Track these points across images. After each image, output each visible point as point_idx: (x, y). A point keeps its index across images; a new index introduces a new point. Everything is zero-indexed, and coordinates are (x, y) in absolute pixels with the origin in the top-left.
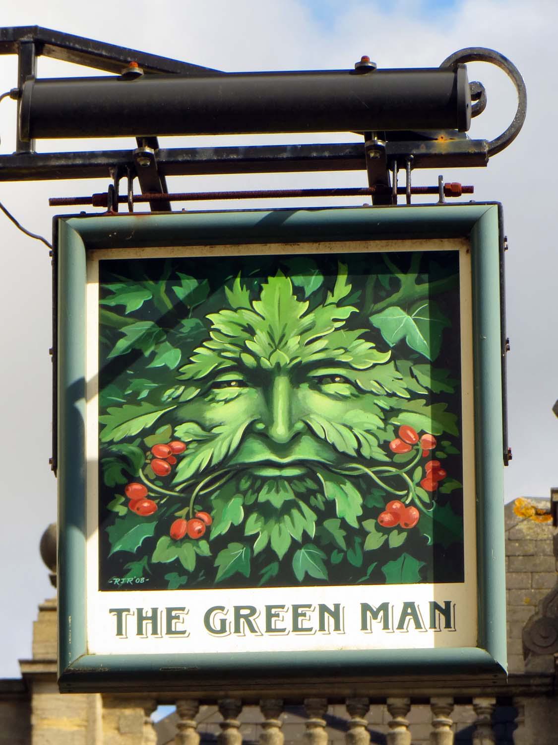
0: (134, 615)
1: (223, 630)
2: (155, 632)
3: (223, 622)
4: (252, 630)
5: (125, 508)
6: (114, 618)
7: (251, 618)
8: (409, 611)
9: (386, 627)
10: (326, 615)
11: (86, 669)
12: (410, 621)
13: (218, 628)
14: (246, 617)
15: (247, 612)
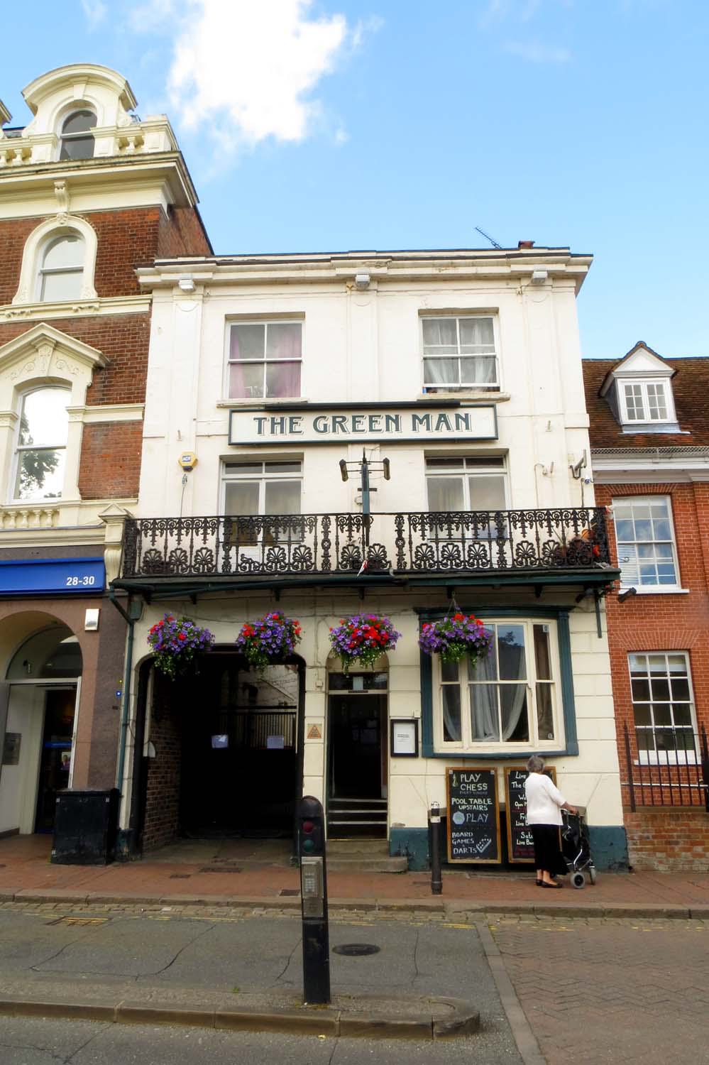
0: (428, 390)
1: (325, 430)
2: (282, 432)
3: (325, 426)
4: (344, 430)
5: (9, 732)
6: (257, 423)
7: (343, 423)
8: (443, 419)
9: (428, 429)
10: (460, 420)
11: (55, 1019)
12: (443, 426)
13: (322, 429)
14: (339, 423)
15: (341, 419)
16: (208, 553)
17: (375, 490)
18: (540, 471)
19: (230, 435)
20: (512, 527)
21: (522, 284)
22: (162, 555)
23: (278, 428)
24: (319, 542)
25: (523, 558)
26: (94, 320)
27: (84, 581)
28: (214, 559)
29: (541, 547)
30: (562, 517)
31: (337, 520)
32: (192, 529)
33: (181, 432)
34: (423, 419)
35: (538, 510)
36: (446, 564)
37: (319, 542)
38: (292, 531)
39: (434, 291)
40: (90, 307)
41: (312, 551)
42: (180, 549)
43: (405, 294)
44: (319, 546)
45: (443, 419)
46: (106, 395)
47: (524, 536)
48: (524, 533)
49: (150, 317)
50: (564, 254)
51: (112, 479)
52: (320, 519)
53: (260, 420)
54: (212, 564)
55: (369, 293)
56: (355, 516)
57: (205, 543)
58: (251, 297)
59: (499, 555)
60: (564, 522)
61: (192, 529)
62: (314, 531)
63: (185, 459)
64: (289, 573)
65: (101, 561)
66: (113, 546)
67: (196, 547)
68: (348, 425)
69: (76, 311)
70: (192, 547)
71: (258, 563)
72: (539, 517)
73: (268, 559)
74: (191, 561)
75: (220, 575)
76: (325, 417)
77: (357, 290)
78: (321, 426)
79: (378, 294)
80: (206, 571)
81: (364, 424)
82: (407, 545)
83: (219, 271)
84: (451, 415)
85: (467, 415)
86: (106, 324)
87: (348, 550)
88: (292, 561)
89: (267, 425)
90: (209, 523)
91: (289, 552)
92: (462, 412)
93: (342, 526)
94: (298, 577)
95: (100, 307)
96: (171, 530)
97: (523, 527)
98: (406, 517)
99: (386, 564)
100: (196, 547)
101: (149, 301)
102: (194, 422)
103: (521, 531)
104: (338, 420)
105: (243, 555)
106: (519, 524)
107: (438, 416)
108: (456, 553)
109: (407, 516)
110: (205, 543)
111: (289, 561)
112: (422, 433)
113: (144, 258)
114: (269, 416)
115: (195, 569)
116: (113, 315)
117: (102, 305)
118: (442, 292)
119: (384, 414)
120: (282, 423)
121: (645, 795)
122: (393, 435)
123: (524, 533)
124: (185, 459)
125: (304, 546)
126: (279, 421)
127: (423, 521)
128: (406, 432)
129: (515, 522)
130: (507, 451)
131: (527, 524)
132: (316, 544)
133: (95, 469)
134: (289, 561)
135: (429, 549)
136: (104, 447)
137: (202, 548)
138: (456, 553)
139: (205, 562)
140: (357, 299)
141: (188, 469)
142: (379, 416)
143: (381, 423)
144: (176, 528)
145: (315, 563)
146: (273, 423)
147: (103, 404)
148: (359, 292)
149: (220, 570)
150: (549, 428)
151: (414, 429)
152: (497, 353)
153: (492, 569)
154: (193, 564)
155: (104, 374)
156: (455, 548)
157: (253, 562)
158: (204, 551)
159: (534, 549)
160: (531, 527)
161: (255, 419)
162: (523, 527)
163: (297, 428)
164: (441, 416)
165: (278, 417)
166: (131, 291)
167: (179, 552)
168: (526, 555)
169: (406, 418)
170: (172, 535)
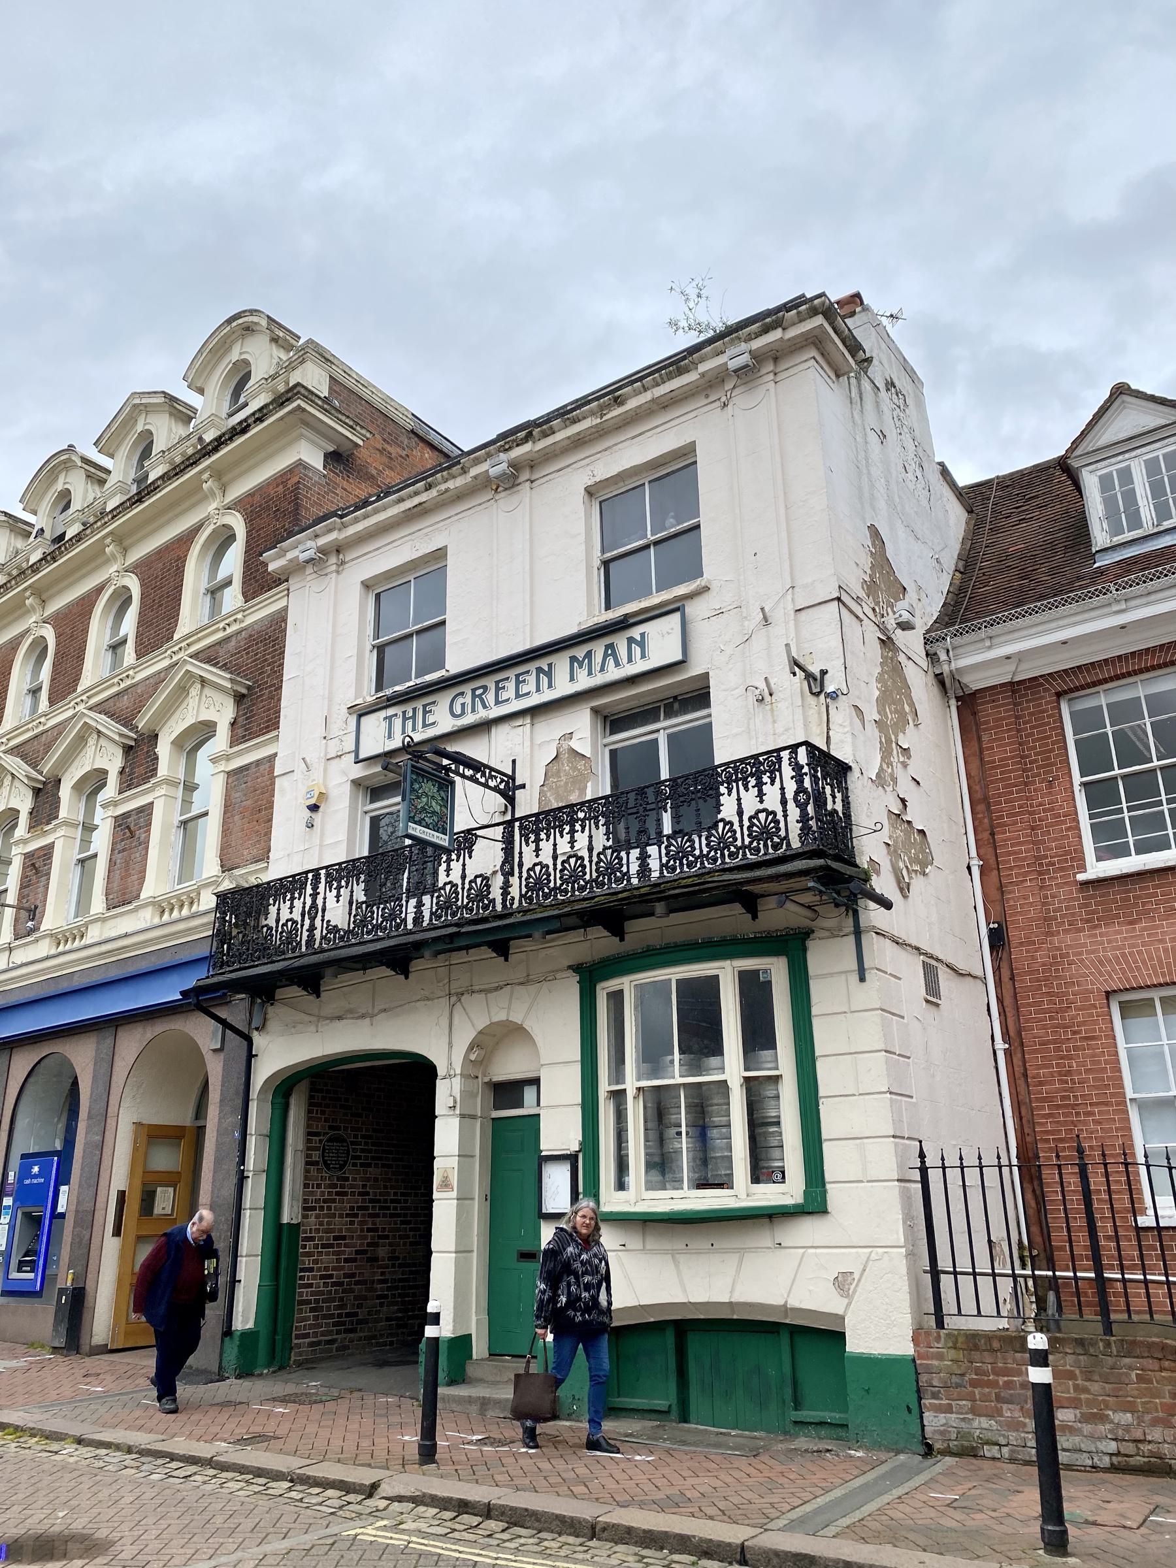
12: (611, 662)
14: (480, 696)
16: (770, 817)
17: (523, 786)
20: (467, 855)
21: (726, 389)
24: (790, 795)
28: (782, 825)
29: (746, 823)
30: (737, 776)
32: (736, 781)
33: (307, 759)
34: (584, 660)
35: (698, 772)
36: (566, 891)
37: (790, 795)
39: (605, 450)
40: (235, 621)
41: (780, 816)
42: (540, 863)
43: (569, 469)
44: (791, 805)
45: (610, 652)
52: (785, 755)
53: (389, 719)
54: (779, 837)
56: (682, 780)
57: (761, 801)
60: (740, 783)
61: (736, 781)
67: (748, 813)
69: (224, 629)
70: (740, 813)
74: (555, 881)
75: (411, 932)
77: (506, 489)
78: (458, 710)
79: (534, 484)
80: (727, 860)
81: (509, 691)
83: (344, 526)
84: (620, 642)
85: (643, 635)
88: (747, 840)
90: (720, 776)
91: (741, 826)
92: (636, 632)
94: (332, 953)
100: (748, 813)
101: (286, 592)
102: (324, 741)
104: (478, 692)
105: (329, 921)
107: (626, 641)
110: (761, 801)
111: (701, 851)
112: (584, 681)
118: (620, 446)
119: (532, 666)
121: (1109, 1225)
122: (548, 696)
125: (722, 820)
128: (564, 687)
130: (706, 676)
132: (784, 802)
134: (701, 851)
136: (244, 798)
137: (535, 865)
139: (765, 834)
140: (505, 502)
141: (314, 808)
144: (752, 775)
145: (787, 837)
148: (508, 492)
149: (410, 926)
150: (765, 619)
153: (630, 889)
154: (705, 850)
155: (247, 702)
156: (770, 817)
158: (762, 816)
163: (431, 719)
164: (607, 647)
167: (762, 816)
170: (747, 789)
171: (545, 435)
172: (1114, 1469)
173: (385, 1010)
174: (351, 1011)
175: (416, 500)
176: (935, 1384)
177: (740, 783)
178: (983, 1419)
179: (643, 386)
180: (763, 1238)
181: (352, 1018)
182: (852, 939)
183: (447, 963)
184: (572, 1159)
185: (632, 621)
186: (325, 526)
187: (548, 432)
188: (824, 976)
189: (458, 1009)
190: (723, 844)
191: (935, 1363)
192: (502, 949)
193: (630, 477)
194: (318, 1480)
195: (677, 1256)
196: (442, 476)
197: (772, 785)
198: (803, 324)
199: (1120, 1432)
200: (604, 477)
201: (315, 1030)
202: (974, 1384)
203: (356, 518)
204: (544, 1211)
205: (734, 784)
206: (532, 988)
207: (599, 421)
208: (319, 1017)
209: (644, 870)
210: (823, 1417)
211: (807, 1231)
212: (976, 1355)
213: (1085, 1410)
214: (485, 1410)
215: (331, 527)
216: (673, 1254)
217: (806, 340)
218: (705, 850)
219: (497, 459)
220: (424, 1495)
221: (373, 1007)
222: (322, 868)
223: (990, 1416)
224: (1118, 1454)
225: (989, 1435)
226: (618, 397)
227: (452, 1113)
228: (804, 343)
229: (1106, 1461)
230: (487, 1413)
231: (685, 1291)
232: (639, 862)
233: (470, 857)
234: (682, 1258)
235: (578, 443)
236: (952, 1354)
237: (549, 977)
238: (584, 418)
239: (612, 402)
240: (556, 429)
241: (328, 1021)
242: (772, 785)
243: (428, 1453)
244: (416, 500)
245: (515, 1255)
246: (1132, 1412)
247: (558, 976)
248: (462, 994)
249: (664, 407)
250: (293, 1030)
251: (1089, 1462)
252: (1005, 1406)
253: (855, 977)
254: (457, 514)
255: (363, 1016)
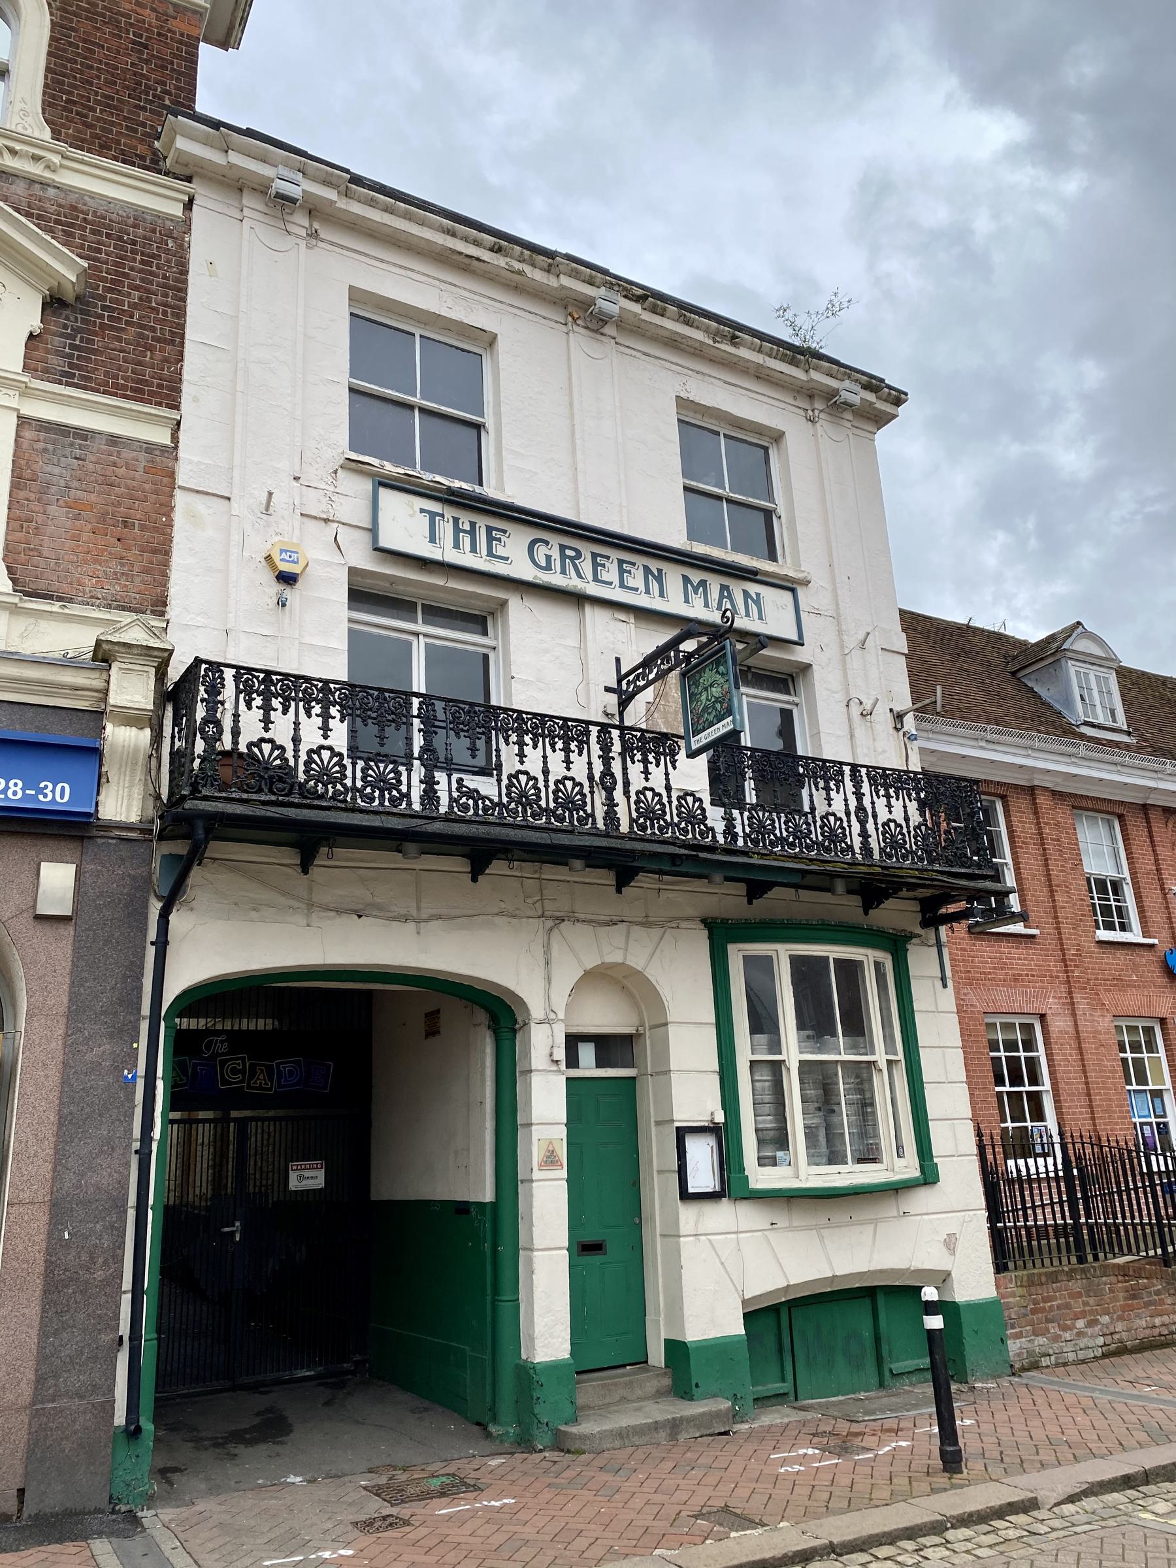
1: (548, 568)
3: (548, 558)
4: (579, 576)
7: (577, 562)
8: (726, 594)
14: (572, 559)
18: (855, 710)
19: (373, 531)
20: (669, 764)
22: (289, 754)
23: (466, 540)
24: (852, 809)
25: (374, 788)
26: (44, 190)
27: (41, 791)
28: (588, 800)
29: (552, 787)
30: (543, 731)
31: (237, 678)
38: (302, 711)
44: (853, 817)
46: (79, 368)
47: (647, 779)
48: (267, 722)
49: (188, 230)
50: (873, 384)
51: (96, 562)
53: (432, 515)
55: (603, 338)
58: (402, 272)
59: (423, 786)
62: (585, 751)
63: (284, 556)
64: (673, 842)
65: (94, 753)
66: (131, 719)
68: (586, 566)
71: (491, 801)
72: (305, 691)
73: (363, 779)
76: (547, 543)
77: (587, 328)
80: (387, 803)
82: (871, 820)
86: (74, 208)
87: (645, 797)
89: (446, 530)
90: (333, 694)
93: (554, 738)
95: (62, 166)
96: (308, 702)
97: (267, 708)
98: (229, 674)
99: (587, 819)
103: (517, 752)
106: (258, 701)
108: (392, 775)
109: (233, 671)
113: (167, 102)
114: (449, 512)
115: (752, 840)
116: (92, 195)
117: (66, 162)
120: (472, 532)
123: (267, 722)
124: (284, 556)
126: (467, 527)
127: (267, 688)
129: (249, 694)
130: (806, 668)
131: (276, 703)
133: (50, 529)
135: (335, 759)
138: (578, 797)
142: (608, 558)
143: (611, 573)
146: (457, 530)
147: (67, 384)
150: (267, 508)
151: (687, 601)
152: (489, 420)
154: (359, 784)
157: (484, 798)
158: (326, 754)
159: (663, 805)
160: (285, 711)
161: (422, 511)
162: (267, 708)
163: (500, 550)
165: (465, 519)
166: (137, 161)
168: (523, 799)
169: (673, 576)
171: (654, 310)
172: (1105, 1356)
173: (440, 918)
174: (379, 907)
175: (472, 250)
176: (1013, 1317)
177: (301, 704)
178: (1040, 1338)
179: (761, 346)
180: (889, 1209)
181: (383, 918)
182: (935, 949)
183: (536, 876)
184: (713, 1129)
185: (758, 577)
186: (327, 172)
187: (659, 310)
188: (923, 977)
189: (556, 936)
190: (798, 834)
191: (1011, 1300)
192: (623, 880)
193: (711, 416)
194: (983, 1513)
195: (822, 1231)
196: (522, 253)
197: (535, 749)
198: (886, 404)
199: (1105, 1330)
200: (697, 400)
201: (304, 922)
202: (1033, 1312)
203: (372, 199)
204: (691, 1190)
205: (293, 704)
206: (656, 932)
207: (711, 342)
208: (311, 905)
209: (430, 795)
210: (917, 1365)
211: (922, 1199)
212: (1033, 1289)
213: (1089, 1318)
214: (677, 1434)
215: (334, 181)
216: (817, 1228)
217: (876, 416)
218: (359, 784)
219: (616, 297)
220: (1093, 1484)
221: (419, 908)
222: (206, 662)
223: (1043, 1335)
224: (1105, 1345)
225: (1043, 1350)
226: (738, 337)
227: (554, 1068)
228: (873, 417)
229: (1099, 1352)
230: (679, 1437)
231: (830, 1263)
232: (423, 786)
233: (675, 768)
234: (825, 1232)
235: (673, 343)
236: (1020, 1291)
237: (672, 923)
238: (697, 328)
239: (729, 336)
240: (667, 314)
241: (332, 914)
242: (535, 749)
243: (952, 1460)
244: (472, 250)
245: (609, 1247)
246: (1108, 1314)
247: (683, 924)
248: (563, 920)
249: (758, 377)
250: (253, 914)
251: (1092, 1355)
252: (1050, 1325)
253: (939, 984)
254: (511, 305)
255: (406, 919)
